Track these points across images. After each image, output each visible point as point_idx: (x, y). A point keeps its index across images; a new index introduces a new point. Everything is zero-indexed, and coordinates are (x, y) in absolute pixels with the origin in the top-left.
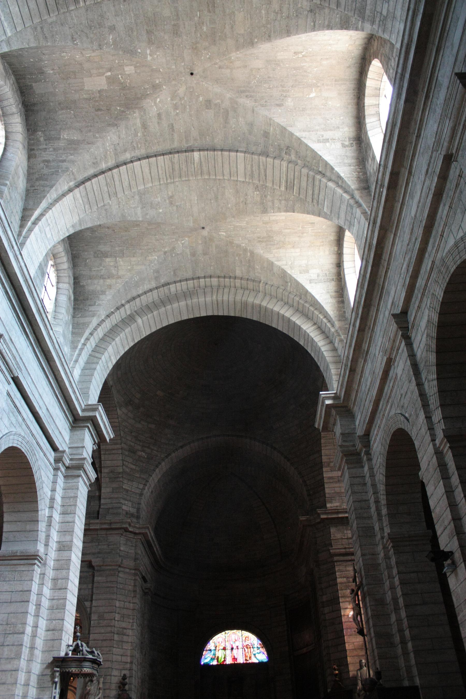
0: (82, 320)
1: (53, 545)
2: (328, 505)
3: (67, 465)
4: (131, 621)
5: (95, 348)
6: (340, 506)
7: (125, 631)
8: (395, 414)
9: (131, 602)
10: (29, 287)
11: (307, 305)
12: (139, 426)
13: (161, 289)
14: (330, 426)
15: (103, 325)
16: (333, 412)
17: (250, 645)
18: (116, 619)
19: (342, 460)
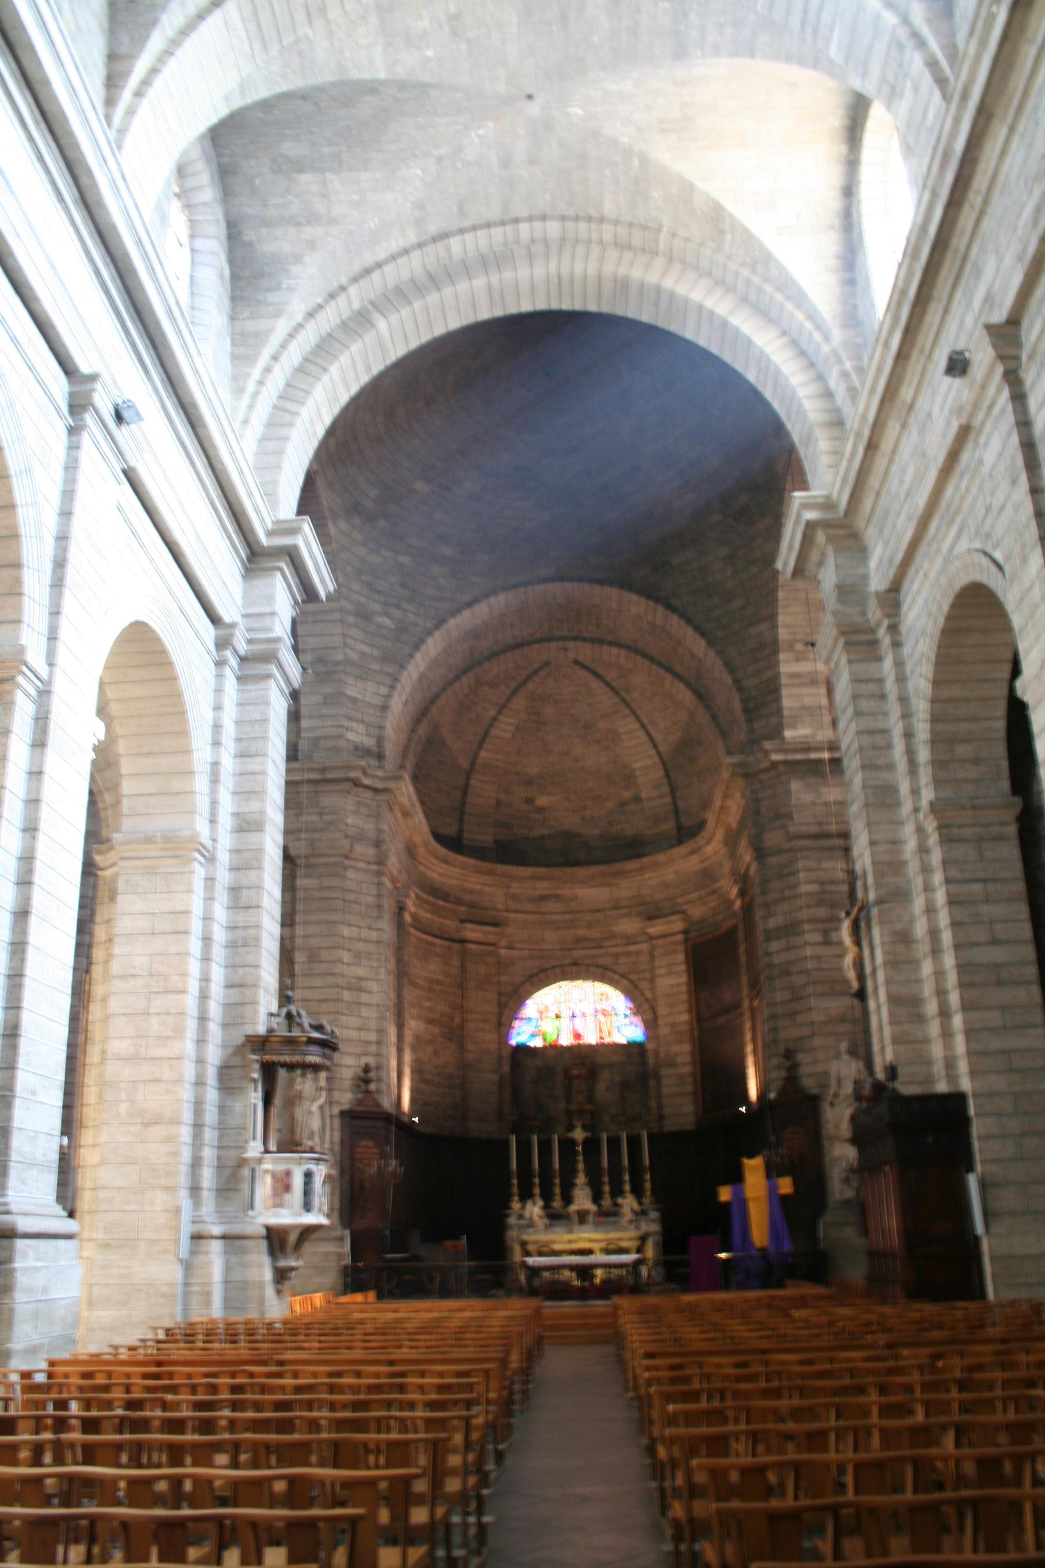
0: (251, 326)
1: (226, 822)
2: (788, 734)
3: (242, 652)
5: (285, 391)
6: (813, 736)
7: (363, 983)
8: (969, 550)
10: (146, 256)
11: (768, 288)
12: (375, 559)
13: (430, 249)
14: (811, 566)
15: (301, 337)
16: (820, 537)
19: (835, 644)
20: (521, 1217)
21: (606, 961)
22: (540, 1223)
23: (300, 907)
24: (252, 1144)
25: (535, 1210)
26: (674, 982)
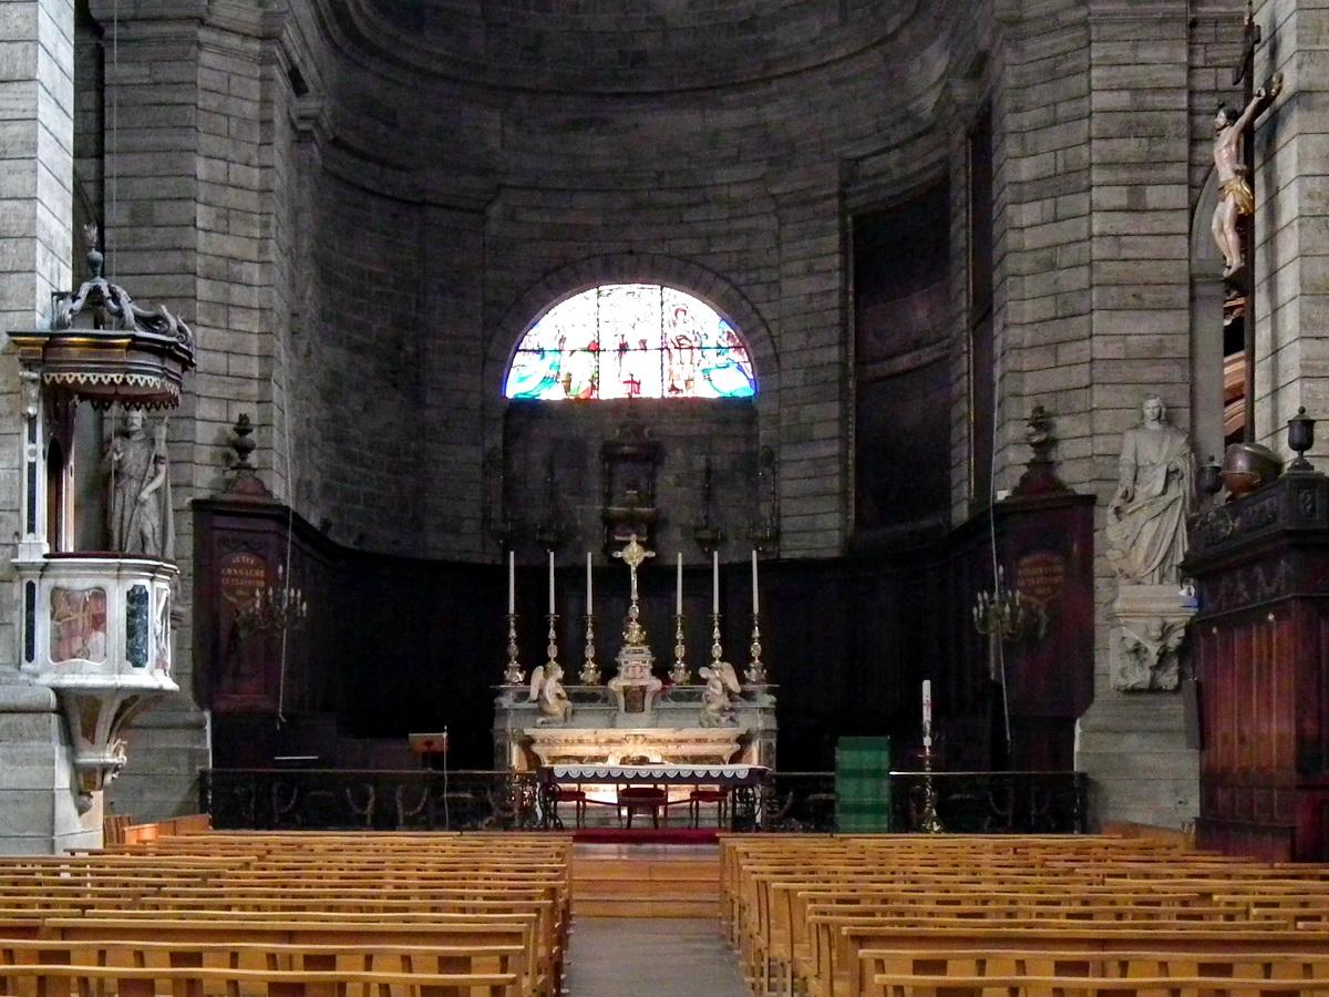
4: (257, 233)
7: (236, 268)
9: (255, 161)
17: (691, 337)
18: (199, 224)
20: (524, 696)
21: (691, 247)
22: (556, 707)
23: (113, 119)
24: (27, 538)
25: (548, 683)
26: (815, 289)
